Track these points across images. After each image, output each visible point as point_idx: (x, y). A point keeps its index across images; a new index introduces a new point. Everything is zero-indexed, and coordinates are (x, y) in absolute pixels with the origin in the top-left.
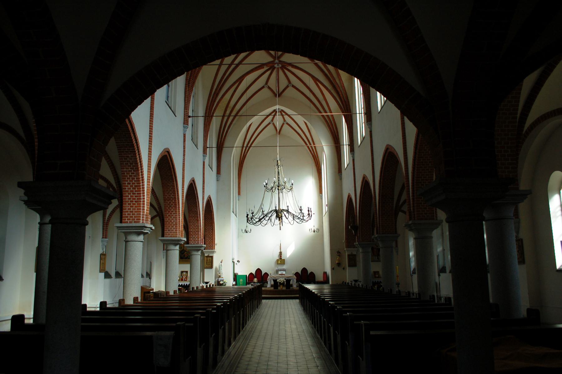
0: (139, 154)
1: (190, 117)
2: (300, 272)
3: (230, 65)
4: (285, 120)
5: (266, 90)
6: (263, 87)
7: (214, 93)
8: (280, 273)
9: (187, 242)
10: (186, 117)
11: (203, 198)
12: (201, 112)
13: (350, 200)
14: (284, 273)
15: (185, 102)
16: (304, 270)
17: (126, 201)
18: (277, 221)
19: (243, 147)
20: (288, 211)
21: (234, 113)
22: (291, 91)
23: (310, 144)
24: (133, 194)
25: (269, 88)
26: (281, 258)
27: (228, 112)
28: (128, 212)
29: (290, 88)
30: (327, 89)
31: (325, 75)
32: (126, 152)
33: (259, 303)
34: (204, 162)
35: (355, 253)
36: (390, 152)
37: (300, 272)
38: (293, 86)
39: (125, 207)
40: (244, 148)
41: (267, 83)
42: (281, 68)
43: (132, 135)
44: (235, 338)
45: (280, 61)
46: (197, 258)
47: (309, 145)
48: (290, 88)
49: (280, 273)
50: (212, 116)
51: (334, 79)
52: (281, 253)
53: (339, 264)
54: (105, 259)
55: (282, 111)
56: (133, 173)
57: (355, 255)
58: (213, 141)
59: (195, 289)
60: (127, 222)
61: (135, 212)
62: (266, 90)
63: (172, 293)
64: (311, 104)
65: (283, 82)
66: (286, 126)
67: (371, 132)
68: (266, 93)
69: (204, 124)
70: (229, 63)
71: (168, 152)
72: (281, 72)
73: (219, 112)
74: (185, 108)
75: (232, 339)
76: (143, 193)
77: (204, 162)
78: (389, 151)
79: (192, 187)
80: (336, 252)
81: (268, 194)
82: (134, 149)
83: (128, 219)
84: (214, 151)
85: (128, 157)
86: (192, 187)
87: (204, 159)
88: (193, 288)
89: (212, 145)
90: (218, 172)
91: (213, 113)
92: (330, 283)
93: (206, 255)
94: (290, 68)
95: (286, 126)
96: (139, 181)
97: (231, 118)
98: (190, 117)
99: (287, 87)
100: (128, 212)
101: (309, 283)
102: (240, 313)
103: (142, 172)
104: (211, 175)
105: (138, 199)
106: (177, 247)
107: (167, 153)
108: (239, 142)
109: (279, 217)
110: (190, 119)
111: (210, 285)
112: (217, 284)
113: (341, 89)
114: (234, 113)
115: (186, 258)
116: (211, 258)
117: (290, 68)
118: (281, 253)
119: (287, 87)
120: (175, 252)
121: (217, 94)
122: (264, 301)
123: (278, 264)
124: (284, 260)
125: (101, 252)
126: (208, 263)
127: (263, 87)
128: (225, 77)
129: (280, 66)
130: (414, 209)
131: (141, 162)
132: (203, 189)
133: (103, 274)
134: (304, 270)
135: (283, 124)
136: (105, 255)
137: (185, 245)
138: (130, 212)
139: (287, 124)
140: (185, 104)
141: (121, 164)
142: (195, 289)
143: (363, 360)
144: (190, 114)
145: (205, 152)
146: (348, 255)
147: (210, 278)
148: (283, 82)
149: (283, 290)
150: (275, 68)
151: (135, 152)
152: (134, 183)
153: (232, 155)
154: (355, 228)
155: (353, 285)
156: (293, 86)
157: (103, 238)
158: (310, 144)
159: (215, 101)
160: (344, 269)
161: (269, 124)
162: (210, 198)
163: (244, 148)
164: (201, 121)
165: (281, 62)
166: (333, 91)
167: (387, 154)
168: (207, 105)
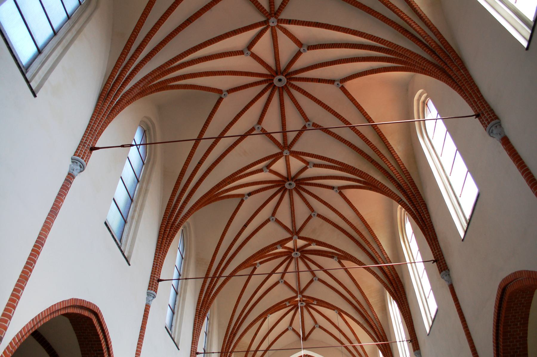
5: (290, 333)
6: (287, 330)
7: (231, 333)
22: (318, 334)
23: (351, 342)
25: (294, 330)
29: (317, 330)
31: (355, 308)
41: (274, 214)
42: (305, 306)
45: (304, 296)
47: (347, 344)
48: (317, 330)
62: (290, 333)
68: (290, 336)
72: (305, 311)
74: (192, 342)
98: (198, 353)
113: (375, 322)
119: (314, 328)
121: (234, 334)
127: (287, 330)
129: (304, 304)
140: (193, 338)
148: (309, 324)
158: (351, 342)
159: (231, 342)
166: (365, 325)
168: (223, 345)
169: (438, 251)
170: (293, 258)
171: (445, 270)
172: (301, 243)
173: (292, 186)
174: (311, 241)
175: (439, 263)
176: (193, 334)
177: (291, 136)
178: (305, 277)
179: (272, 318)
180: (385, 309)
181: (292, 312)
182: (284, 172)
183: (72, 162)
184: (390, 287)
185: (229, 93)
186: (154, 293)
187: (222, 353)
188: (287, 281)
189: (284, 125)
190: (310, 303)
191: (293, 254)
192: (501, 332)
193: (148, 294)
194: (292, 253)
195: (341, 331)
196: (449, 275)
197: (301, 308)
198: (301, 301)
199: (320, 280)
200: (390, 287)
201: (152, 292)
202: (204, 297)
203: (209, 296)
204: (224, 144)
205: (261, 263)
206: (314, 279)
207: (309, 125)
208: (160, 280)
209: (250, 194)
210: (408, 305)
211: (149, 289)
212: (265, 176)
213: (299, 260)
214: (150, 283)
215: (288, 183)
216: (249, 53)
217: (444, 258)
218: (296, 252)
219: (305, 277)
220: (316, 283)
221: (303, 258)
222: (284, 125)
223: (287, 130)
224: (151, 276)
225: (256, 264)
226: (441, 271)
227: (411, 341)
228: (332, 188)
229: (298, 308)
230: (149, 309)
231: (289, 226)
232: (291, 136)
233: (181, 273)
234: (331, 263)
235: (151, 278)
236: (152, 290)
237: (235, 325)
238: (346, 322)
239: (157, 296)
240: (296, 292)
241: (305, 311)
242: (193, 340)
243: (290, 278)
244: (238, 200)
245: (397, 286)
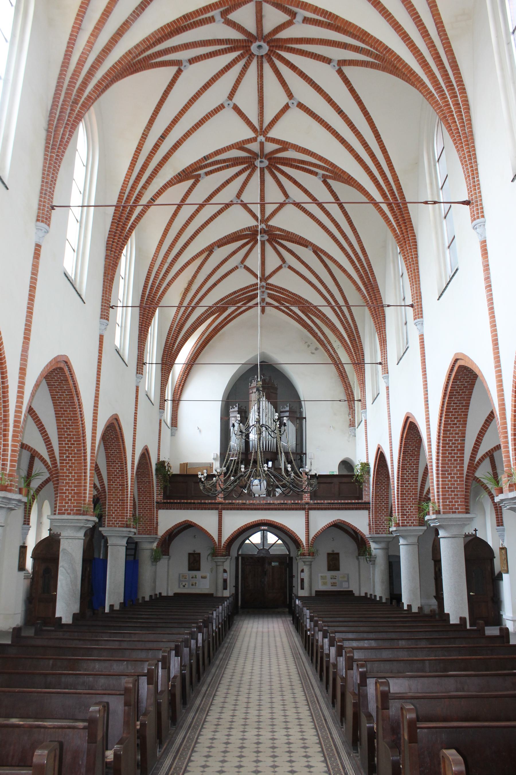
3: (201, 206)
19: (179, 307)
29: (295, 113)
38: (301, 106)
48: (295, 113)
119: (287, 107)
127: (221, 107)
156: (301, 106)
163: (183, 309)
172: (270, 147)
173: (261, 50)
174: (285, 146)
177: (269, 209)
178: (275, 98)
179: (220, 254)
182: (251, 27)
183: (37, 229)
185: (190, 64)
189: (262, 197)
190: (276, 237)
193: (160, 413)
195: (340, 112)
197: (262, 170)
199: (290, 267)
205: (207, 174)
206: (283, 265)
207: (292, 103)
209: (192, 61)
212: (218, 30)
213: (266, 172)
215: (258, 43)
216: (243, 266)
218: (259, 160)
219: (275, 98)
220: (285, 271)
222: (262, 197)
223: (266, 202)
225: (199, 175)
228: (328, 61)
229: (255, 167)
231: (255, 122)
232: (269, 209)
238: (326, 266)
240: (254, 129)
241: (268, 177)
243: (251, 194)
244: (174, 69)
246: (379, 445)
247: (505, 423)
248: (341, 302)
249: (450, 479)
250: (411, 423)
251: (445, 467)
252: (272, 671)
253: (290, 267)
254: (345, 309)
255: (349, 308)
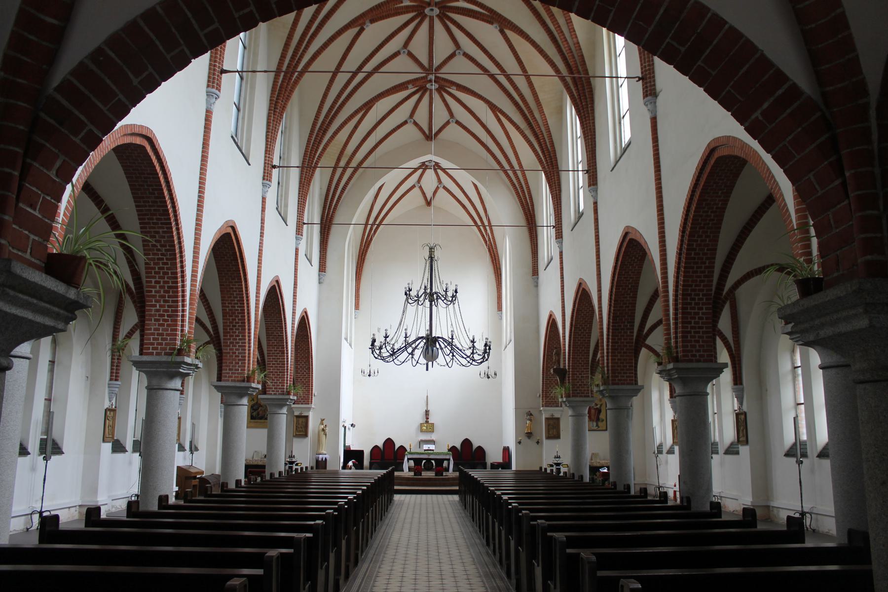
0: (178, 229)
1: (274, 167)
2: (458, 446)
3: (355, 74)
4: (440, 181)
5: (410, 127)
6: (405, 122)
8: (426, 447)
9: (264, 391)
10: (269, 167)
11: (294, 313)
12: (295, 159)
13: (552, 323)
14: (432, 447)
15: (267, 141)
16: (467, 443)
17: (151, 315)
18: (423, 360)
19: (366, 224)
20: (450, 344)
21: (354, 164)
24: (165, 301)
25: (416, 124)
26: (427, 422)
27: (342, 163)
28: (153, 334)
29: (453, 126)
30: (517, 128)
31: (516, 104)
32: (154, 223)
33: (390, 500)
34: (297, 250)
35: (556, 416)
36: (631, 240)
37: (458, 446)
38: (458, 123)
39: (149, 325)
40: (369, 226)
43: (166, 193)
44: (347, 577)
46: (282, 420)
48: (453, 126)
49: (426, 447)
50: (315, 167)
51: (531, 112)
52: (427, 413)
53: (529, 435)
54: (114, 418)
55: (437, 166)
56: (167, 264)
57: (558, 419)
58: (313, 212)
59: (277, 476)
60: (152, 354)
61: (167, 335)
63: (232, 486)
64: (489, 155)
65: (440, 115)
66: (441, 191)
67: (595, 203)
69: (300, 182)
70: (354, 70)
71: (233, 228)
73: (328, 159)
74: (266, 151)
75: (341, 582)
76: (183, 301)
77: (297, 250)
78: (629, 237)
79: (274, 294)
80: (525, 415)
81: (412, 309)
82: (170, 219)
83: (153, 349)
84: (317, 229)
85: (158, 233)
86: (274, 294)
87: (297, 244)
88: (272, 475)
89: (312, 219)
90: (322, 268)
91: (317, 163)
92: (514, 468)
93: (297, 413)
94: (454, 91)
95: (441, 191)
96: (177, 278)
97: (349, 171)
98: (274, 167)
99: (448, 123)
100: (153, 334)
101: (474, 467)
102: (358, 529)
103: (182, 262)
104: (309, 272)
105: (172, 311)
106: (245, 401)
107: (230, 230)
108: (359, 215)
109: (430, 354)
110: (275, 172)
111: (302, 469)
112: (314, 465)
114: (354, 164)
115: (261, 418)
116: (304, 420)
117: (454, 91)
118: (427, 413)
119: (448, 123)
120: (243, 410)
121: (324, 130)
122: (397, 497)
123: (422, 431)
124: (433, 424)
125: (107, 405)
126: (300, 427)
127: (405, 122)
128: (337, 106)
130: (676, 342)
131: (180, 243)
132: (295, 296)
133: (109, 445)
134: (467, 443)
135: (437, 188)
136: (114, 411)
137: (260, 396)
138: (158, 335)
139: (445, 188)
140: (267, 144)
141: (144, 246)
142: (277, 476)
143: (555, 588)
144: (276, 162)
145: (299, 231)
146: (547, 419)
147: (304, 457)
148: (440, 115)
149: (430, 474)
150: (426, 90)
151: (171, 224)
152: (168, 282)
153: (346, 241)
154: (562, 373)
155: (548, 471)
156: (458, 123)
157: (111, 380)
160: (538, 443)
161: (413, 187)
162: (306, 313)
163: (369, 226)
164: (294, 176)
165: (437, 80)
166: (528, 132)
167: (625, 244)
168: (307, 146)
169: (649, 65)
170: (426, 16)
171: (650, 94)
175: (646, 83)
176: (267, 138)
178: (443, 46)
180: (561, 112)
181: (417, 97)
184: (573, 89)
186: (217, 92)
187: (278, 72)
188: (414, 53)
191: (427, 11)
192: (696, 198)
194: (425, 8)
196: (655, 103)
198: (430, 81)
199: (466, 55)
200: (573, 89)
201: (214, 90)
202: (283, 81)
203: (290, 79)
204: (360, 76)
206: (457, 52)
208: (223, 71)
210: (594, 119)
211: (208, 86)
213: (437, 22)
214: (209, 77)
217: (654, 77)
221: (442, 17)
224: (210, 65)
226: (645, 95)
227: (587, 171)
230: (211, 117)
233: (247, 45)
234: (488, 33)
235: (210, 69)
236: (213, 87)
237: (326, 116)
239: (222, 94)
241: (437, 22)
242: (266, 147)
245: (584, 90)
246: (551, 311)
247: (667, 291)
248: (516, 167)
249: (698, 348)
250: (584, 289)
251: (173, 302)
252: (430, 566)
253: (466, 55)
254: (519, 173)
255: (523, 171)
